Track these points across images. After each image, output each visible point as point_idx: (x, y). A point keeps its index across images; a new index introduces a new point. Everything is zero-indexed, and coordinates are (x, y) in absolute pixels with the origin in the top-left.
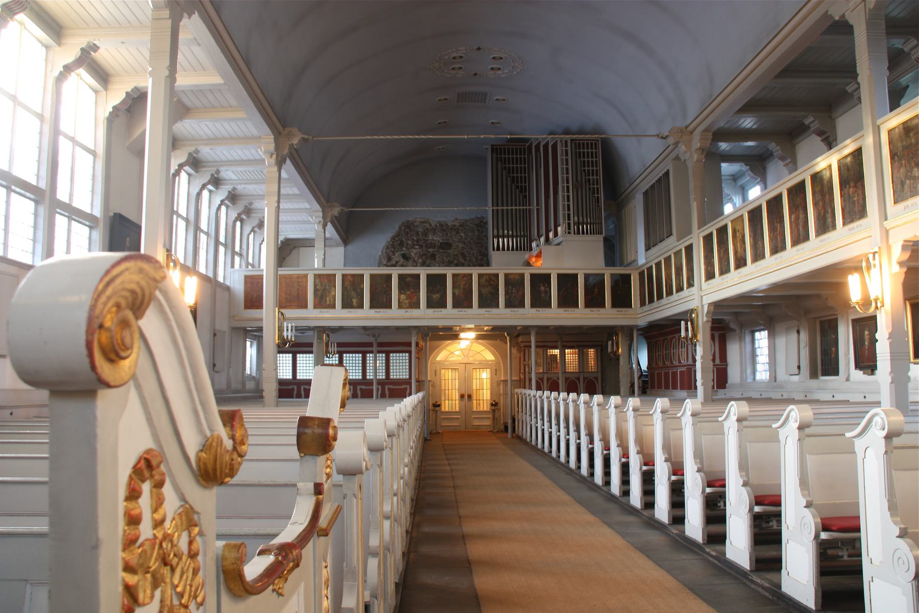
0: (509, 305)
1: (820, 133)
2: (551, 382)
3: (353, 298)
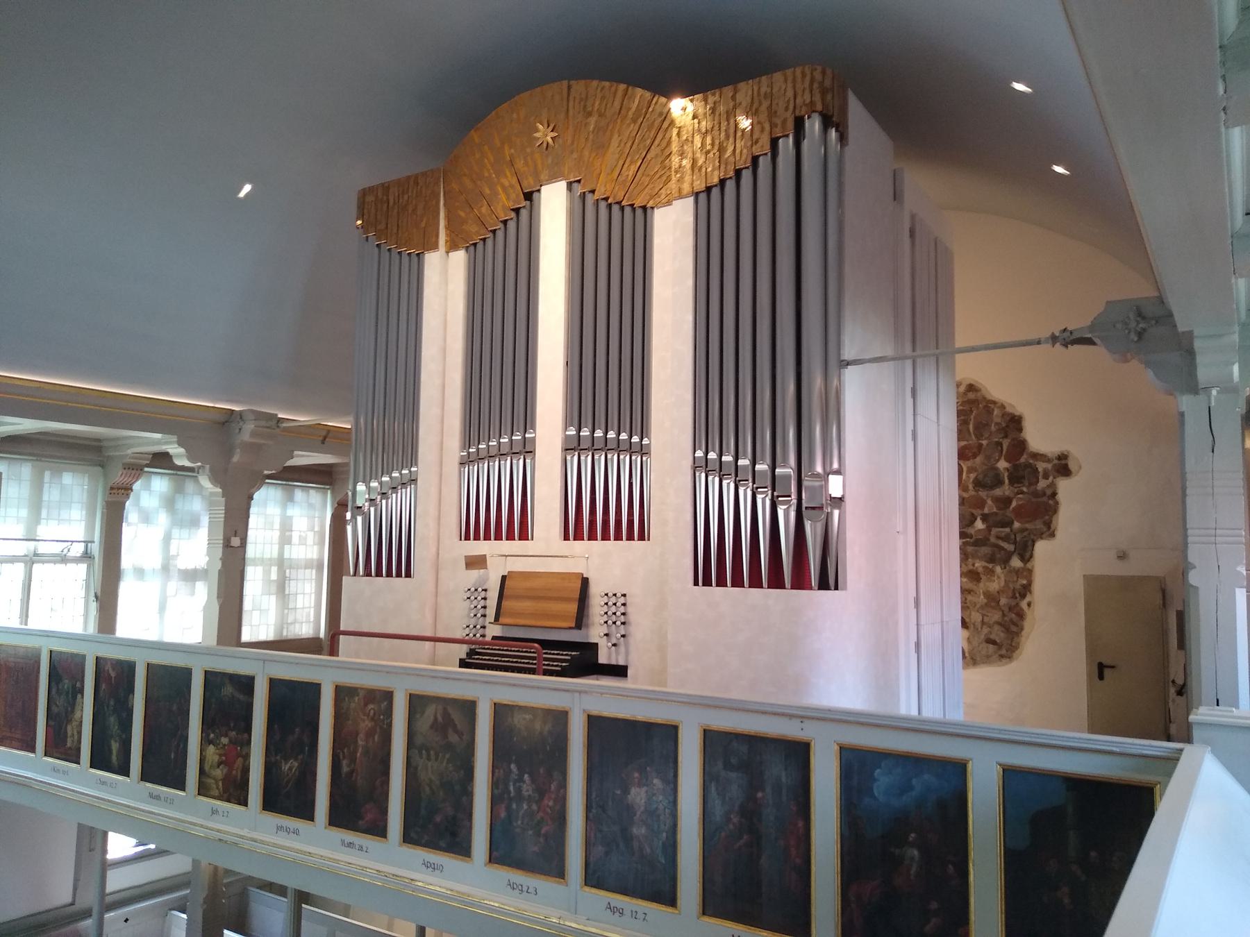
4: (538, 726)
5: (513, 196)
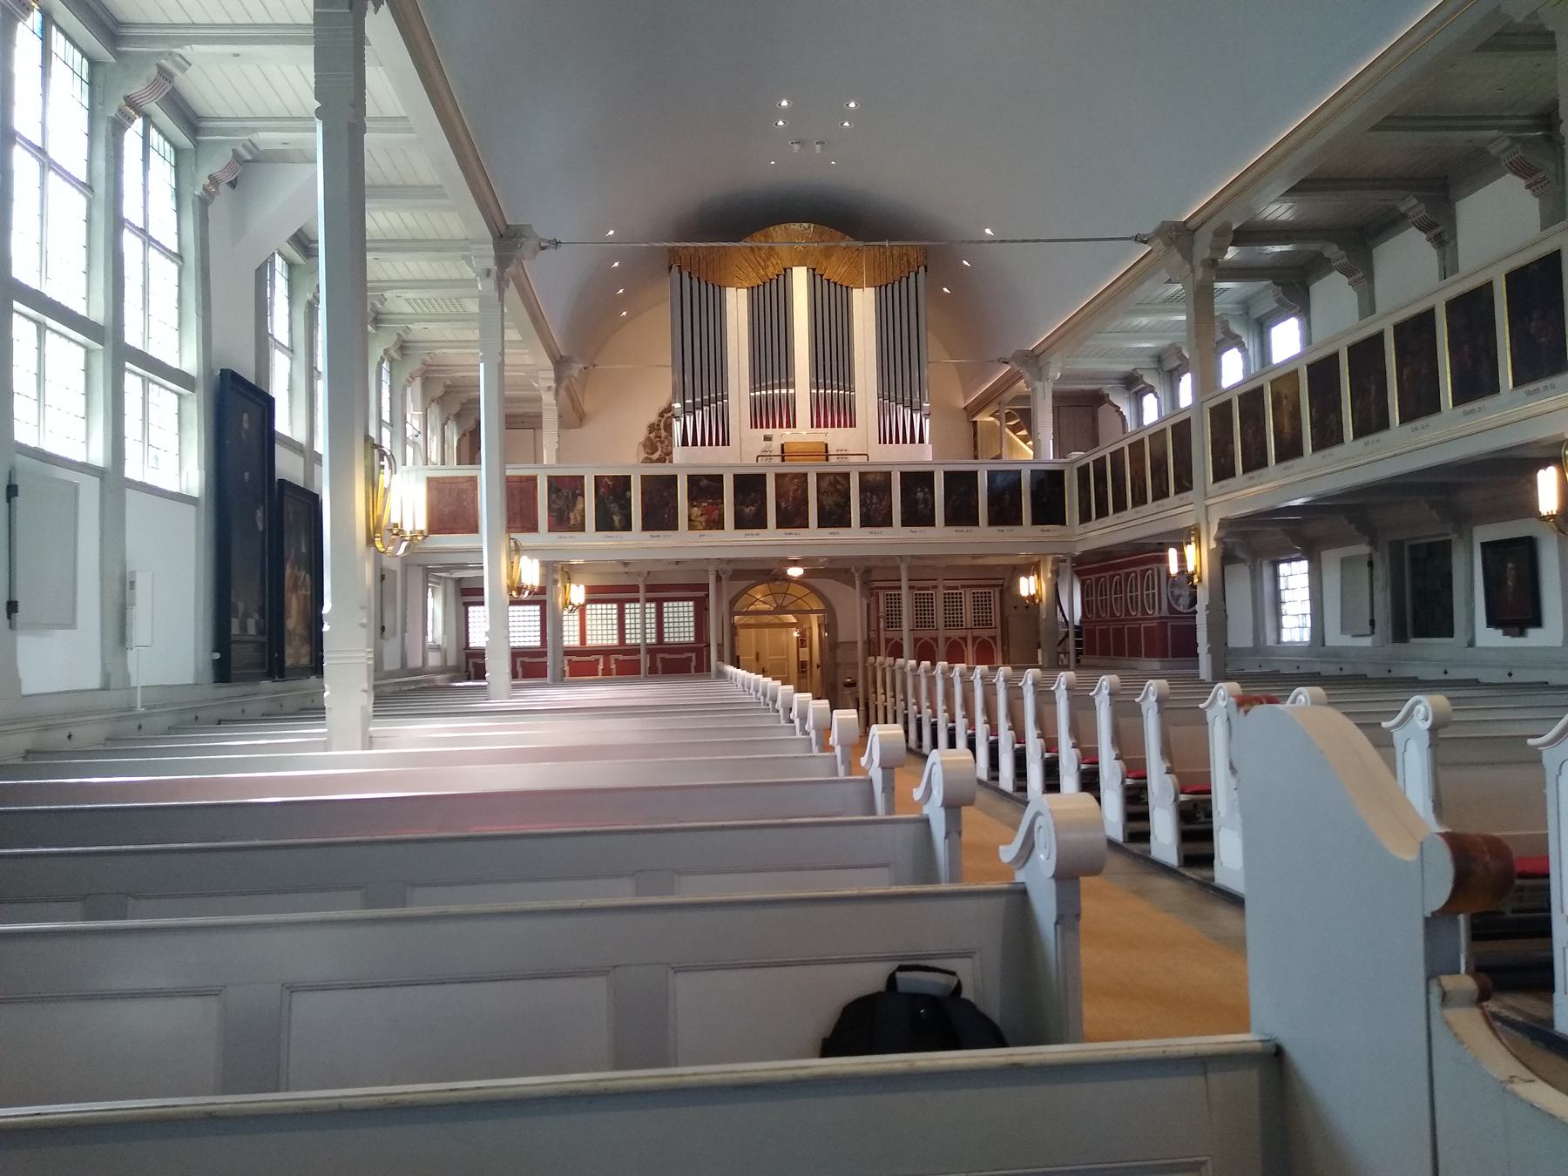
0: (866, 521)
1: (1424, 227)
2: (932, 645)
3: (614, 514)
4: (878, 478)
5: (778, 269)
